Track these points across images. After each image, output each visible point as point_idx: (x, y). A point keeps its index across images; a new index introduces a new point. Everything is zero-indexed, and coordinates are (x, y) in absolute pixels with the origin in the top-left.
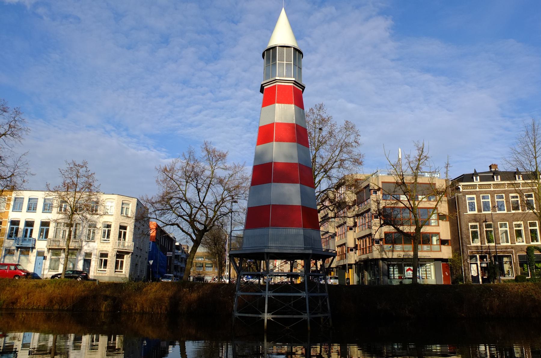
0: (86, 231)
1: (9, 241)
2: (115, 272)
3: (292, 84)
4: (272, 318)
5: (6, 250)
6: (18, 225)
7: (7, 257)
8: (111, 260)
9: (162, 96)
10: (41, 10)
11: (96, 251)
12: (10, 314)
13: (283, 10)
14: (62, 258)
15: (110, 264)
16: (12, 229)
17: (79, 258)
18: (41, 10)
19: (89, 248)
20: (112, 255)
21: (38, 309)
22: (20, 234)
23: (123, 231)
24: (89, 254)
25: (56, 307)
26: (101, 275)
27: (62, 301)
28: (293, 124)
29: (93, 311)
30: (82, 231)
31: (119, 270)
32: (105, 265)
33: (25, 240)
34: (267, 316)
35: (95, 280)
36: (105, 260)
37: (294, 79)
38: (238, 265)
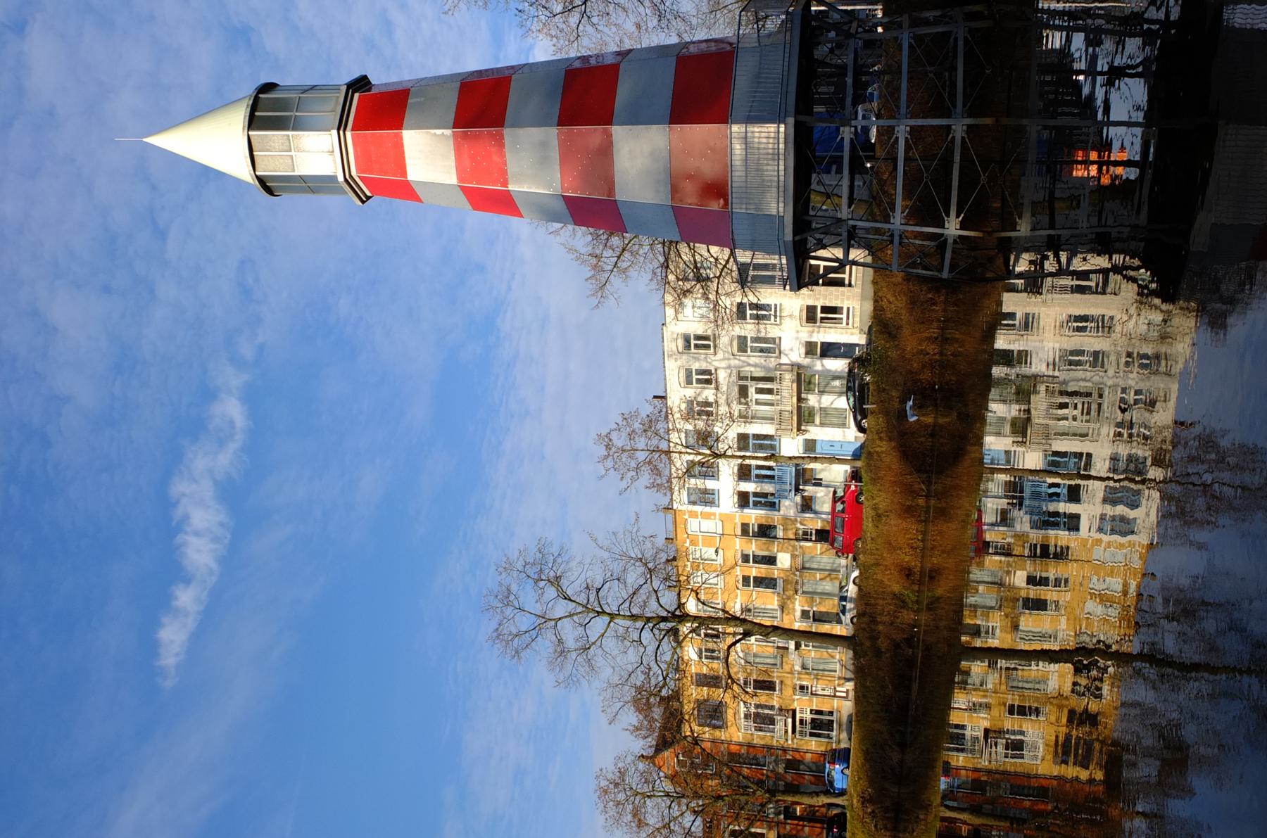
0: (755, 359)
1: (782, 508)
2: (850, 285)
3: (348, 134)
4: (958, 217)
5: (803, 511)
6: (747, 493)
8: (820, 296)
11: (801, 335)
12: (931, 578)
13: (152, 140)
14: (819, 402)
15: (830, 300)
16: (756, 504)
18: (247, 350)
19: (796, 349)
20: (809, 296)
21: (924, 533)
22: (768, 488)
24: (810, 348)
25: (921, 501)
26: (857, 319)
27: (910, 491)
29: (932, 435)
30: (755, 366)
32: (834, 310)
33: (780, 478)
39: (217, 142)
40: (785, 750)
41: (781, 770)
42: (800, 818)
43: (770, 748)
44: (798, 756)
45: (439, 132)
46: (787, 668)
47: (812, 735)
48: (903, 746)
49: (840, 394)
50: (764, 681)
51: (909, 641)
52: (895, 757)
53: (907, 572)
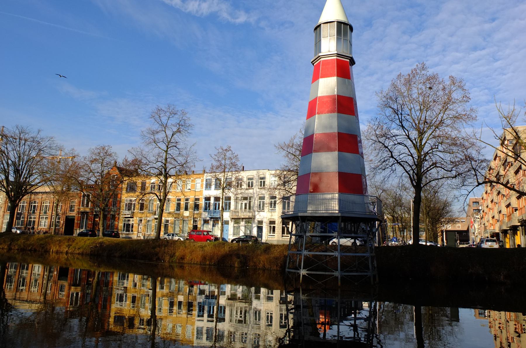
3: (335, 57)
5: (204, 220)
6: (264, 199)
7: (205, 225)
8: (279, 226)
9: (371, 74)
10: (263, 24)
16: (206, 203)
17: (254, 225)
18: (263, 24)
21: (197, 264)
22: (212, 208)
24: (260, 222)
26: (271, 239)
28: (335, 95)
31: (285, 235)
32: (274, 231)
34: (303, 272)
35: (266, 243)
40: (119, 214)
41: (111, 213)
42: (94, 220)
43: (120, 209)
44: (116, 219)
45: (336, 90)
46: (148, 215)
47: (124, 224)
49: (245, 233)
52: (117, 254)
53: (183, 258)
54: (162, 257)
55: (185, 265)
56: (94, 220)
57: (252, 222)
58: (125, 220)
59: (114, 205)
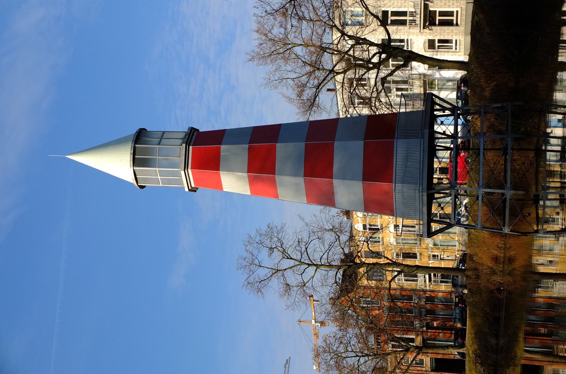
2: (457, 25)
3: (190, 171)
15: (444, 36)
20: (430, 34)
23: (391, 18)
26: (462, 47)
31: (454, 18)
36: (438, 42)
37: (183, 172)
38: (445, 226)
39: (117, 164)
40: (425, 291)
41: (423, 303)
42: (436, 328)
43: (414, 290)
44: (433, 295)
45: (240, 174)
46: (424, 246)
47: (441, 282)
48: (497, 337)
49: (453, 90)
50: (409, 253)
51: (499, 290)
52: (493, 341)
53: (496, 259)
54: (495, 285)
55: (508, 255)
56: (436, 328)
57: (431, 78)
58: (435, 281)
59: (410, 298)
